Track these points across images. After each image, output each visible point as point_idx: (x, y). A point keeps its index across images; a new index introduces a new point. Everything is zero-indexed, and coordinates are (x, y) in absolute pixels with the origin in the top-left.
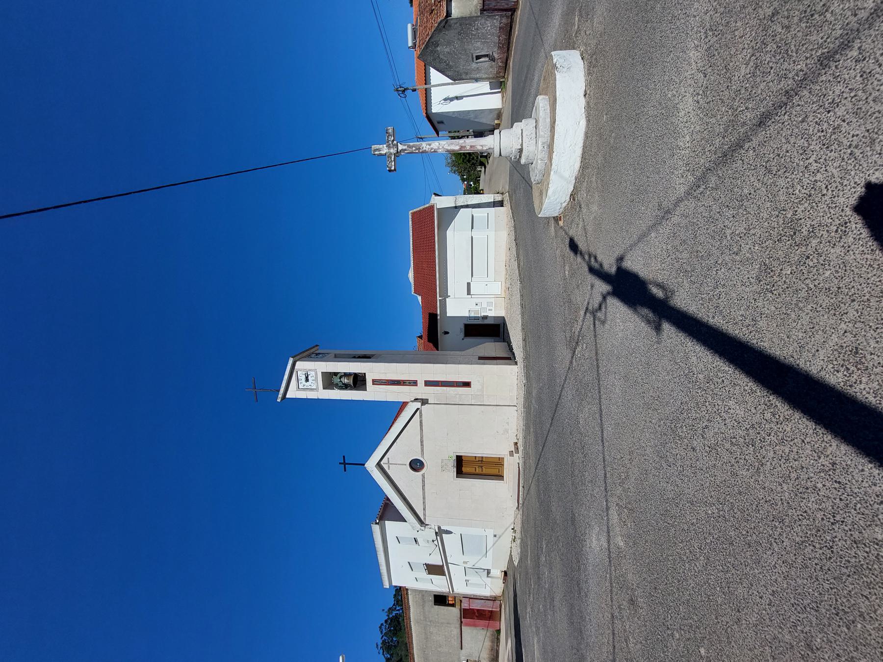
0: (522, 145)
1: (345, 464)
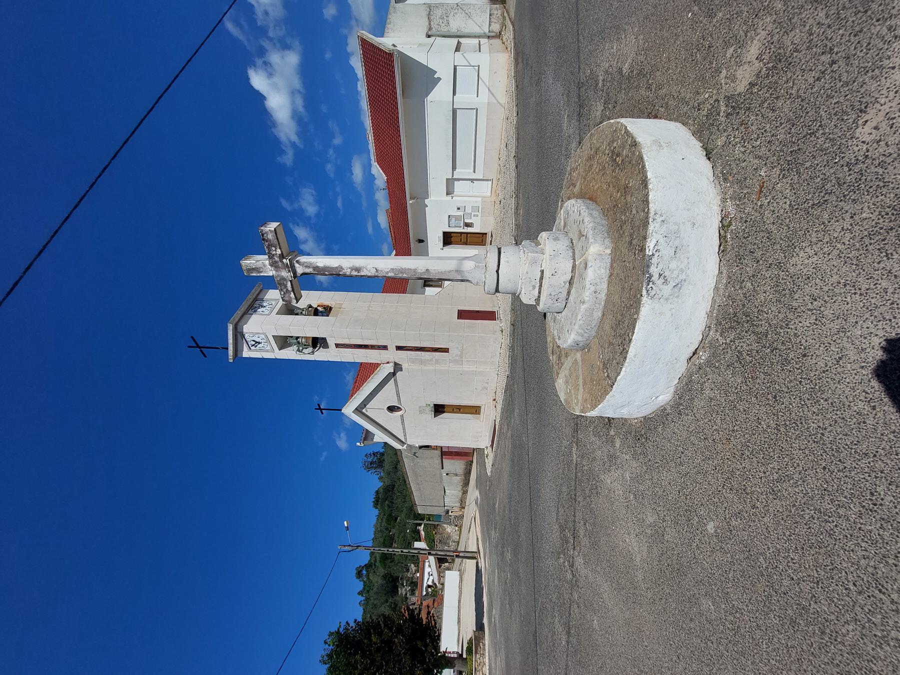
0: (538, 300)
1: (321, 410)
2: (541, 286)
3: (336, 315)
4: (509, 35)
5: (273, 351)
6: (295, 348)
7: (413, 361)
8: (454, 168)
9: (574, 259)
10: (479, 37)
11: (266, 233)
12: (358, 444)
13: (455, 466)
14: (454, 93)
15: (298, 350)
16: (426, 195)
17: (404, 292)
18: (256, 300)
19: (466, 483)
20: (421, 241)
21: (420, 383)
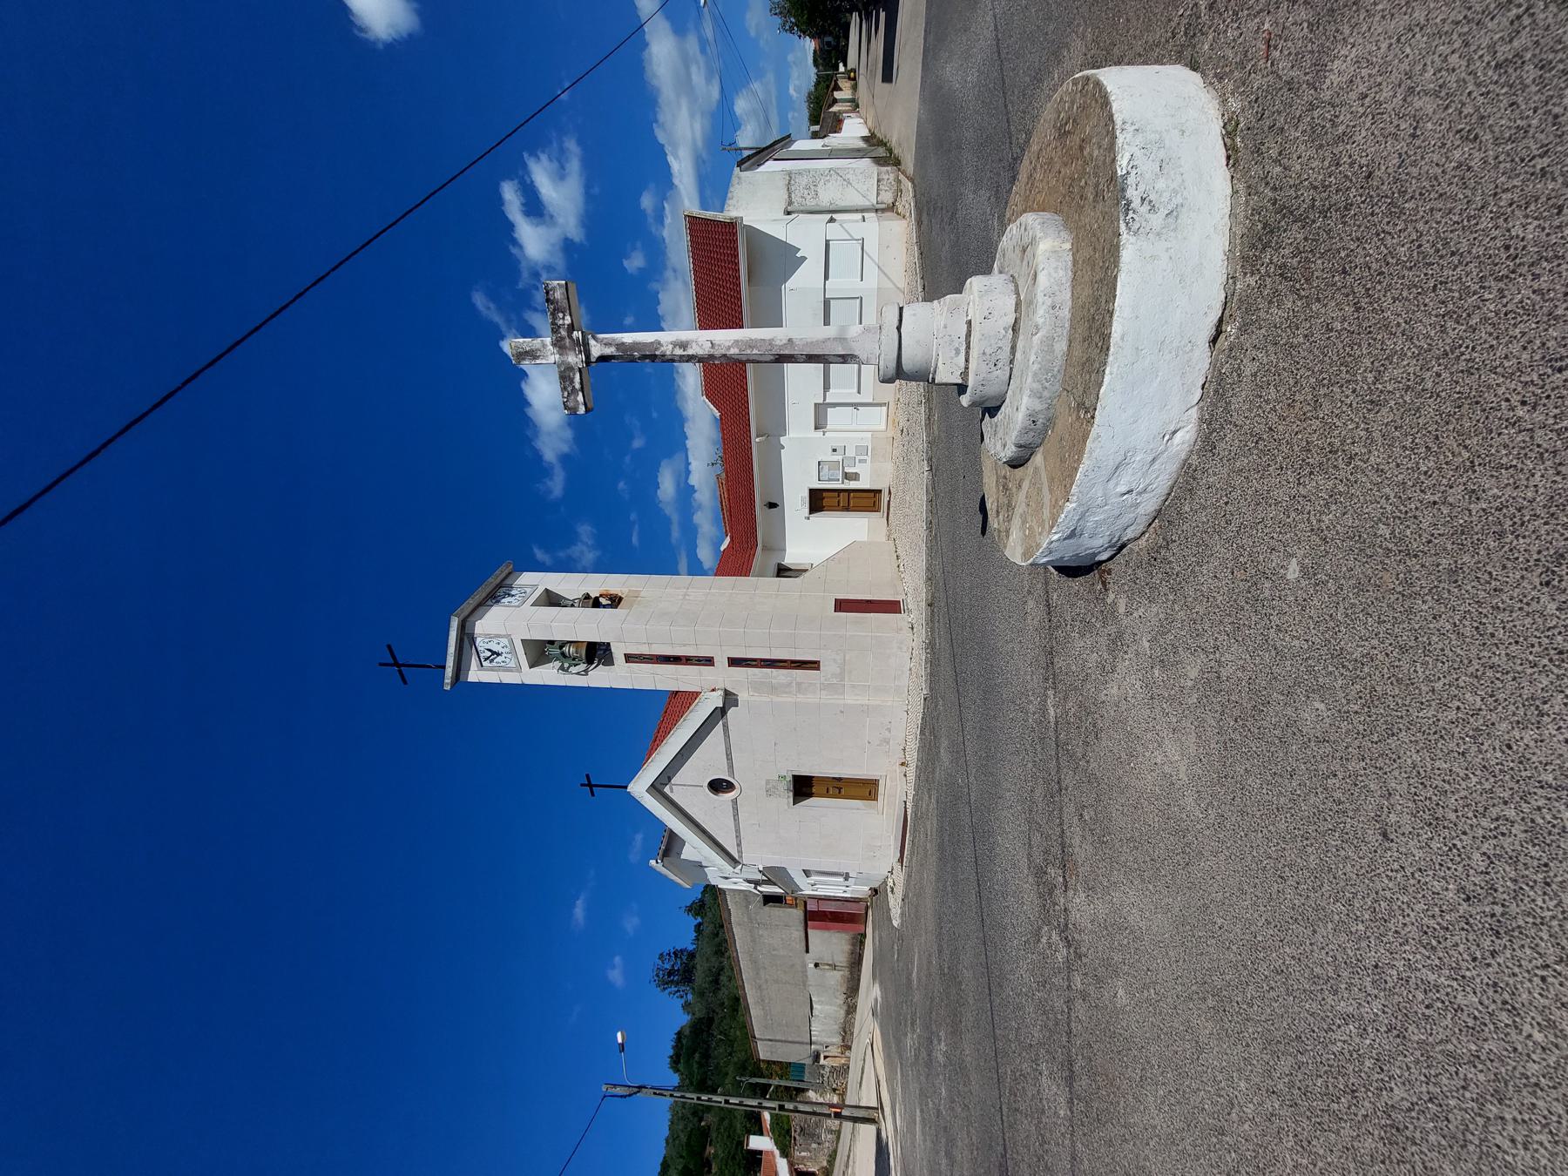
0: (965, 374)
1: (590, 785)
2: (968, 347)
3: (630, 607)
4: (907, 202)
5: (519, 668)
6: (558, 664)
7: (757, 687)
8: (826, 387)
9: (1018, 294)
10: (862, 211)
11: (554, 289)
12: (653, 862)
13: (830, 944)
14: (826, 277)
15: (562, 668)
16: (782, 430)
17: (747, 574)
18: (500, 586)
19: (853, 989)
20: (772, 505)
21: (772, 732)
